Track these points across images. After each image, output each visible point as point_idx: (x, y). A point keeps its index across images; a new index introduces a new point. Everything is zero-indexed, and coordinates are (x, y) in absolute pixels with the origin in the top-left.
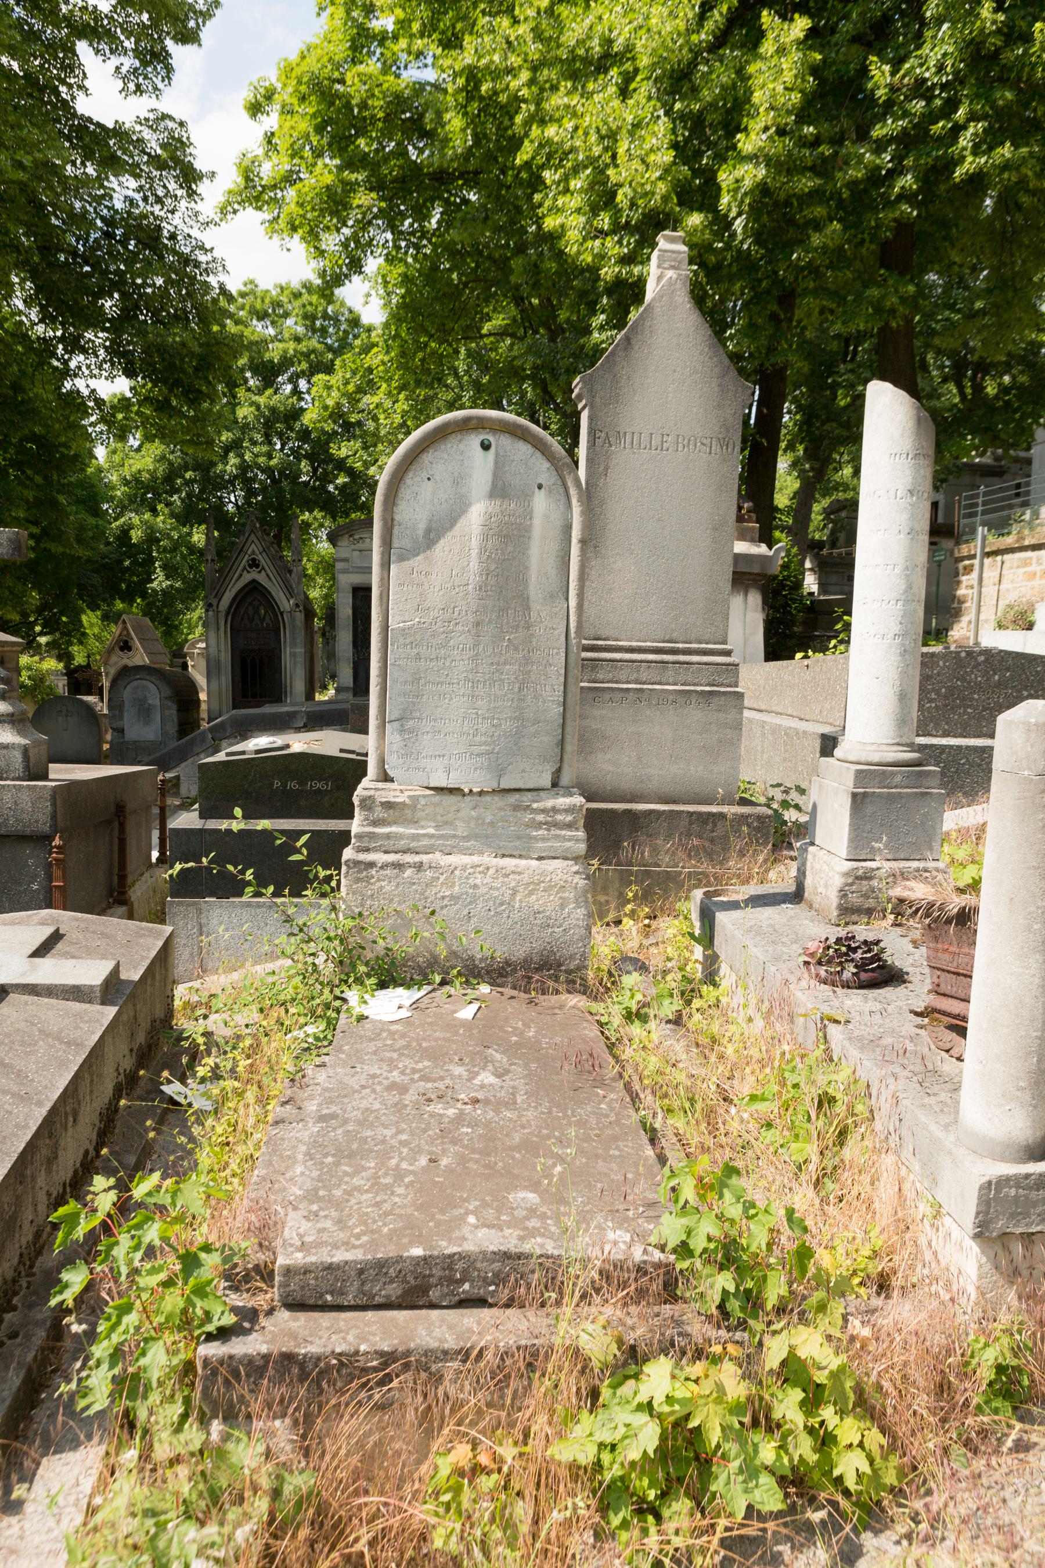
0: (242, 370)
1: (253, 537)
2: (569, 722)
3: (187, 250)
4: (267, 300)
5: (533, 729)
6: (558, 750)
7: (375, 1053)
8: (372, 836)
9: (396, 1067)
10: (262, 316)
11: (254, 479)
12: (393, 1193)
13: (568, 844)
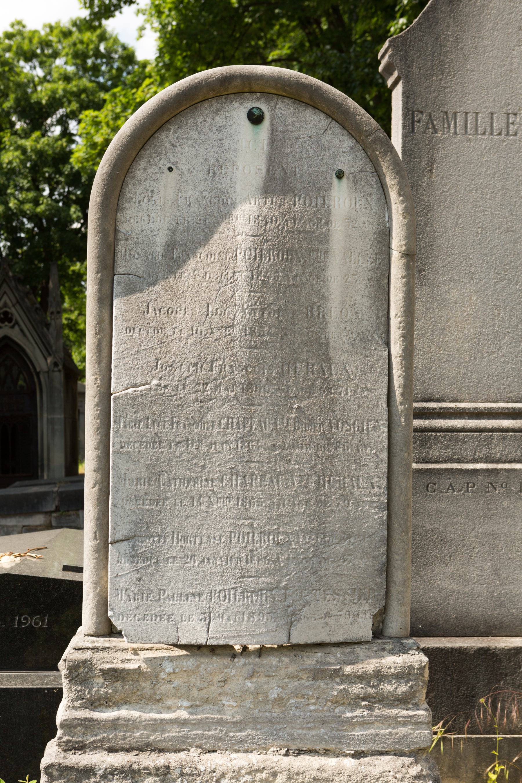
0: (8, 114)
2: (397, 535)
4: (35, 41)
5: (340, 548)
6: (381, 580)
8: (89, 725)
10: (29, 57)
11: (21, 228)
13: (403, 730)
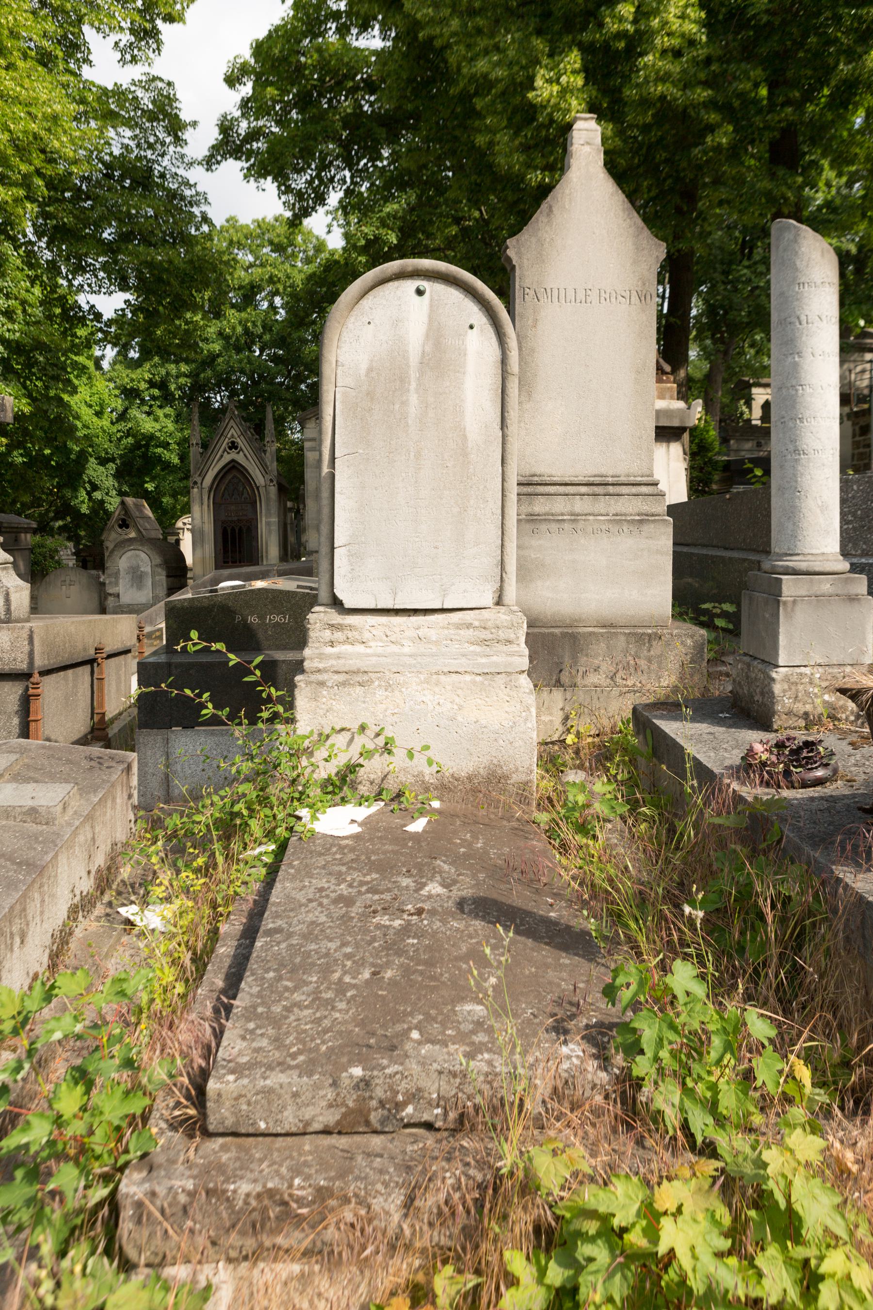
1: (232, 423)
3: (174, 186)
6: (498, 570)
7: (324, 867)
9: (345, 880)
11: (237, 381)
12: (333, 1008)
